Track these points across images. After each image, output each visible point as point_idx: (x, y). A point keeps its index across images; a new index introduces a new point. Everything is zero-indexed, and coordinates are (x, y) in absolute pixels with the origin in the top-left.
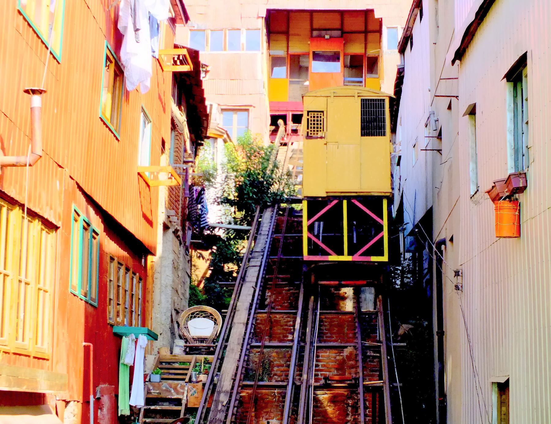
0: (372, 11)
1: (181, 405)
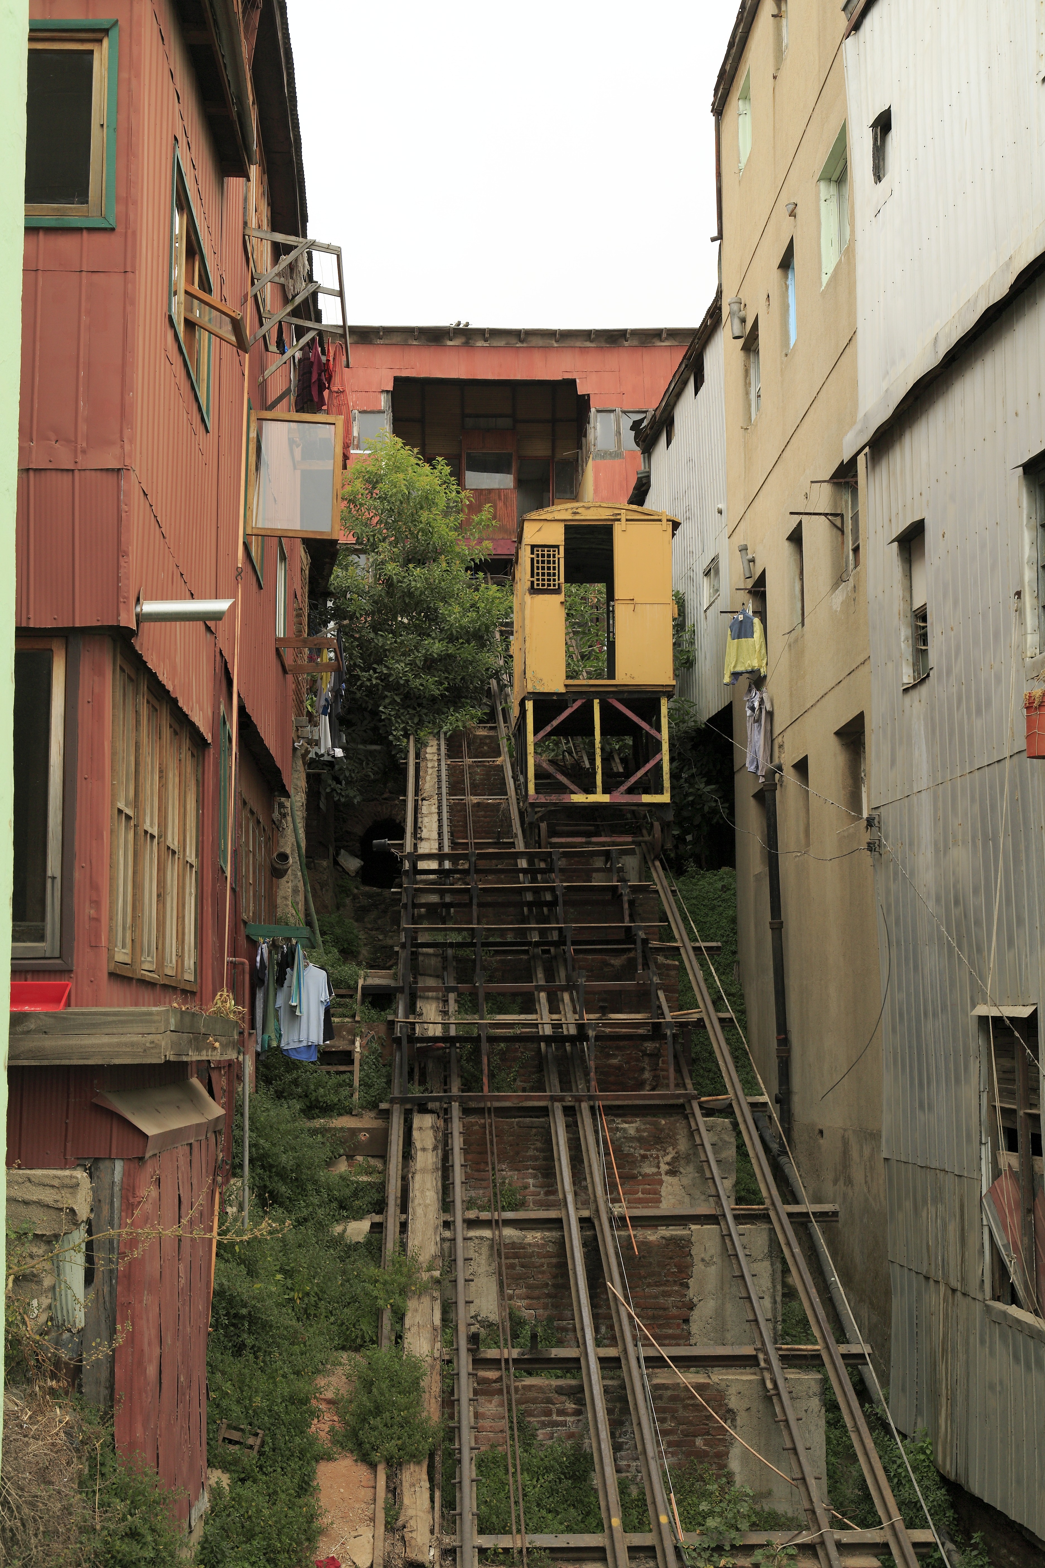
0: (572, 383)
1: (352, 1062)
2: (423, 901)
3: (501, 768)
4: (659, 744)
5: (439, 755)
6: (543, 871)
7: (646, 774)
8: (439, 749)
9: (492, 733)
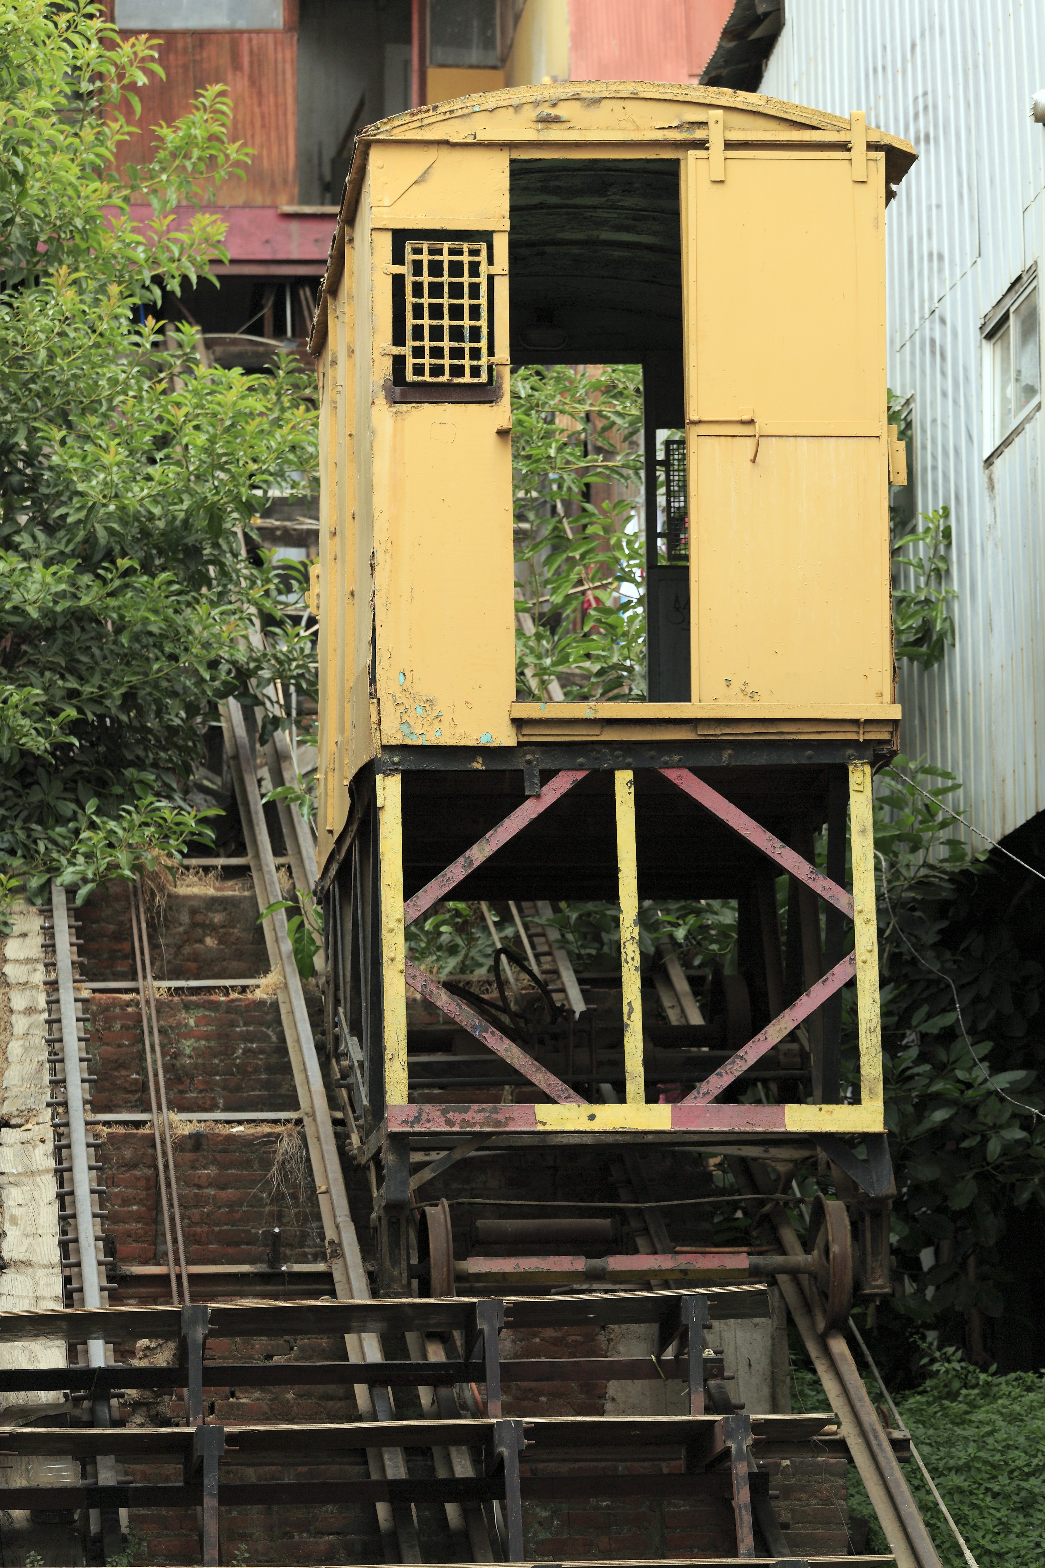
2: (19, 1482)
3: (269, 1014)
4: (842, 929)
5: (50, 966)
6: (437, 1376)
7: (792, 1036)
8: (50, 947)
9: (233, 890)
